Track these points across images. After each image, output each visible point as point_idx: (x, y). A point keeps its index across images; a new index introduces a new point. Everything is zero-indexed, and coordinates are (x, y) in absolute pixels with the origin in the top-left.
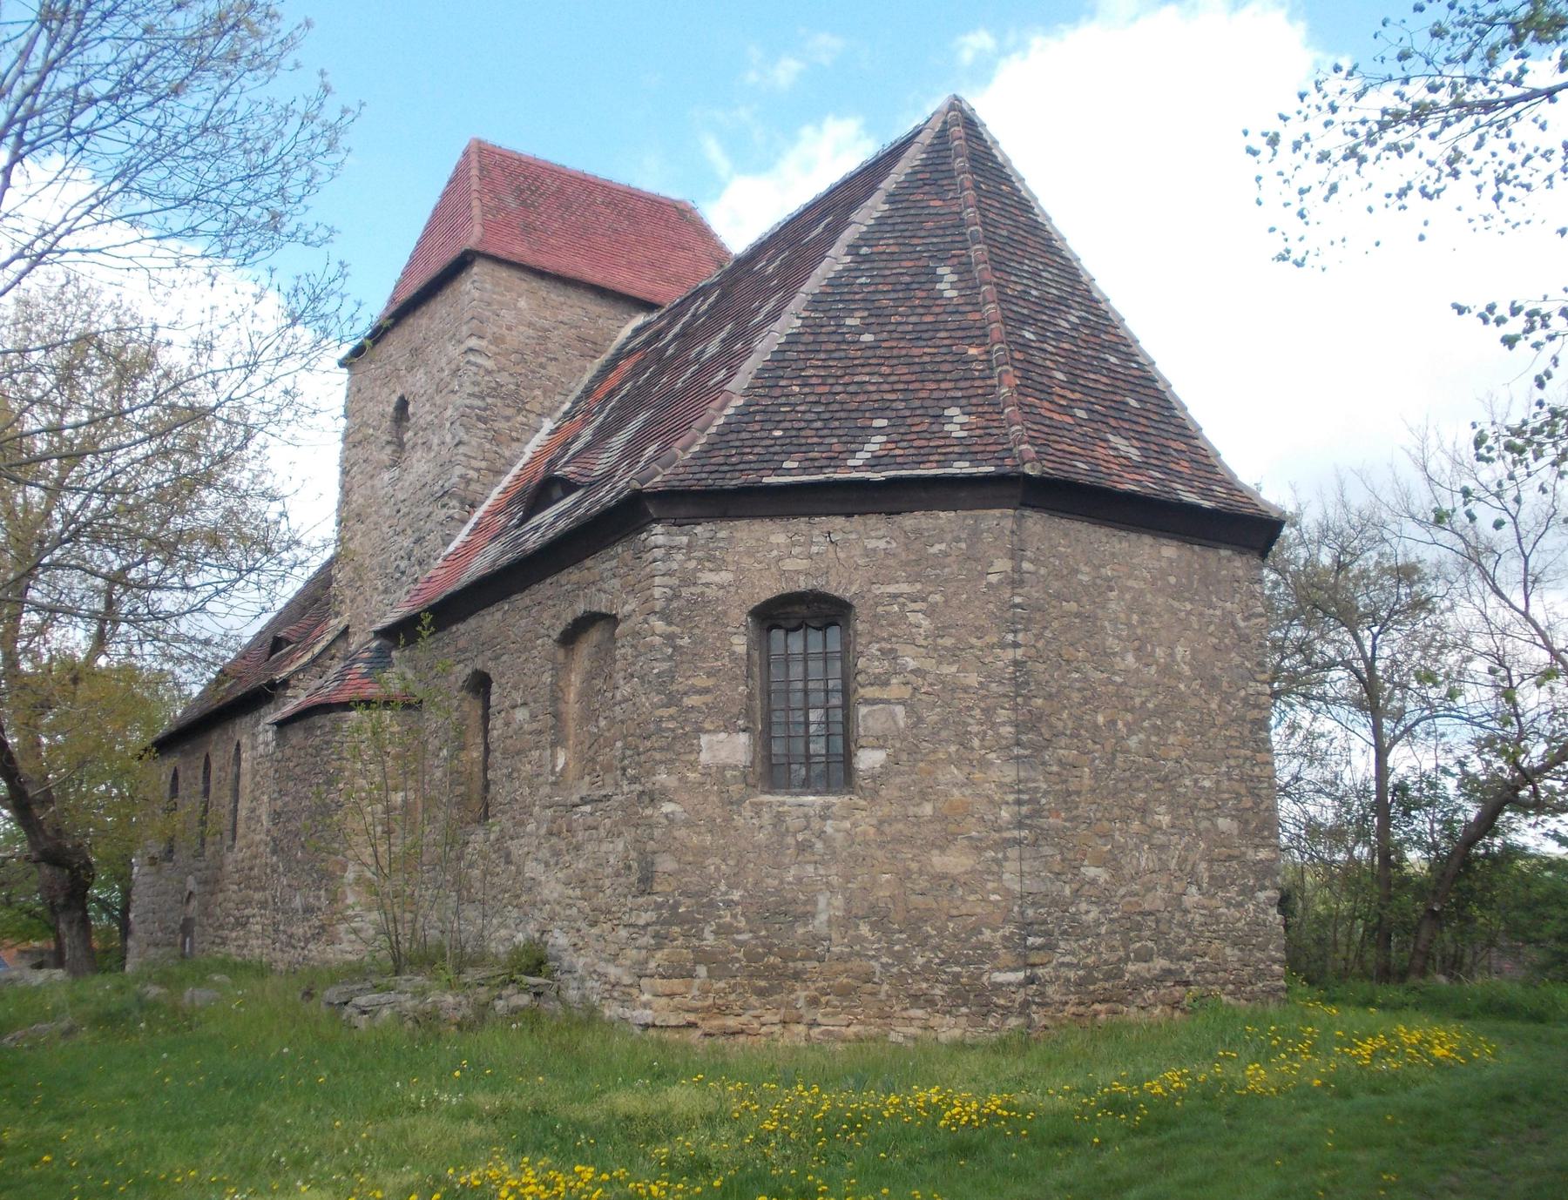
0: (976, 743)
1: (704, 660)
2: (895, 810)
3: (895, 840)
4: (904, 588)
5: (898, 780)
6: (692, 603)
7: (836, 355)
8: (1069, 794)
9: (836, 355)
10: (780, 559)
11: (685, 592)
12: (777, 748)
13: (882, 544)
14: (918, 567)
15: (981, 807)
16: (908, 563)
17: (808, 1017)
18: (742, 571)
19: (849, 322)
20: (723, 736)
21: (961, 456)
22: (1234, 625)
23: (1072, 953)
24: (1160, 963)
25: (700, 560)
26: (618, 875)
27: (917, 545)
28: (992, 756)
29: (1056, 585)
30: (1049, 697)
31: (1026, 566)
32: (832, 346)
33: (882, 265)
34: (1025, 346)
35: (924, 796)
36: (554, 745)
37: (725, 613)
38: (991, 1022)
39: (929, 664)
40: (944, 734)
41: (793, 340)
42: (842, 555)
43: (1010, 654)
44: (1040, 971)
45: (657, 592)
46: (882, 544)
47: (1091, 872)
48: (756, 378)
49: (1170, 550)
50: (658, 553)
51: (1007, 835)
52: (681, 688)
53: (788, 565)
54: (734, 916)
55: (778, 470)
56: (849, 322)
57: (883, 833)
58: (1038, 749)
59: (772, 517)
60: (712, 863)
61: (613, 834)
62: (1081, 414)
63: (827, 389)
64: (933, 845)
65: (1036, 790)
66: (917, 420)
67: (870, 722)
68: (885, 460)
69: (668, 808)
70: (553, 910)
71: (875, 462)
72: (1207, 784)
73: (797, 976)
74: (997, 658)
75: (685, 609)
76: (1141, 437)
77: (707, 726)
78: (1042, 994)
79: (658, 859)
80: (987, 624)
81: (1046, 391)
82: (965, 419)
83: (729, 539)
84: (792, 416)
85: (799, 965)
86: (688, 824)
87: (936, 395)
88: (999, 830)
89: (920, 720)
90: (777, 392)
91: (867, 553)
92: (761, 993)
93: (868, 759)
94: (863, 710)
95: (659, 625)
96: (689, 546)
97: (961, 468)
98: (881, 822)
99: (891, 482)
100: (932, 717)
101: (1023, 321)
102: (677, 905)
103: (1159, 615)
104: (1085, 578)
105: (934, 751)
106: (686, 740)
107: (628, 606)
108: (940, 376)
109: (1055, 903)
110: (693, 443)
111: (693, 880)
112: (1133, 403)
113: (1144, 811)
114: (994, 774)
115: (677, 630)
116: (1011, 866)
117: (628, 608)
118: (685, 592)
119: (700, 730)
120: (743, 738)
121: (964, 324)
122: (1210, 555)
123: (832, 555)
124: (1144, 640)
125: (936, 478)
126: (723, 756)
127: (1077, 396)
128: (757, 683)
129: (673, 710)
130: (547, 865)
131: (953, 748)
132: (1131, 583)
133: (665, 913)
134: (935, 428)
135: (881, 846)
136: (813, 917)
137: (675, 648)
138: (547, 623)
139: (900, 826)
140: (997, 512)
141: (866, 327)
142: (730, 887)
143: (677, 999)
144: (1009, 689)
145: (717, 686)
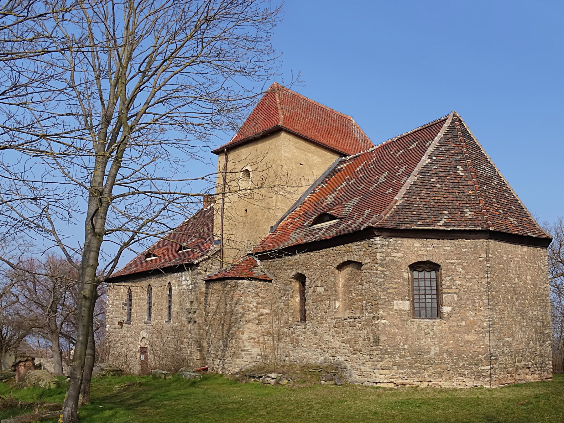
0: (477, 305)
1: (394, 279)
2: (454, 323)
3: (454, 332)
4: (456, 261)
5: (455, 315)
6: (390, 262)
7: (430, 190)
8: (501, 318)
9: (430, 190)
10: (418, 251)
11: (387, 258)
12: (417, 305)
13: (449, 248)
14: (459, 255)
15: (479, 322)
16: (456, 254)
17: (429, 380)
18: (406, 254)
19: (432, 180)
20: (401, 301)
21: (471, 224)
22: (541, 268)
23: (502, 361)
24: (523, 363)
25: (392, 249)
26: (364, 340)
27: (459, 249)
28: (482, 308)
29: (498, 260)
30: (496, 292)
31: (490, 255)
32: (428, 187)
33: (440, 163)
34: (484, 191)
35: (463, 320)
36: (335, 300)
37: (401, 266)
38: (481, 379)
39: (464, 283)
40: (468, 302)
41: (415, 184)
42: (437, 251)
43: (486, 280)
44: (494, 366)
45: (378, 258)
46: (449, 248)
47: (506, 339)
48: (405, 194)
49: (525, 249)
50: (378, 246)
51: (486, 330)
52: (387, 287)
53: (420, 253)
54: (405, 353)
55: (416, 225)
56: (432, 180)
57: (451, 330)
58: (494, 306)
59: (415, 238)
60: (398, 338)
61: (363, 328)
62: (501, 211)
63: (428, 200)
64: (465, 333)
65: (494, 317)
66: (457, 212)
67: (447, 299)
68: (449, 224)
69: (383, 321)
70: (337, 350)
71: (446, 224)
72: (535, 313)
73: (425, 369)
74: (483, 281)
75: (389, 264)
76: (517, 217)
77: (396, 298)
78: (495, 372)
79: (381, 336)
80: (480, 272)
81: (491, 205)
82: (470, 213)
83: (401, 244)
84: (418, 208)
85: (426, 366)
86: (390, 326)
87: (461, 205)
88: (484, 328)
89: (461, 298)
90: (412, 200)
91: (444, 250)
92: (413, 374)
93: (446, 309)
94: (444, 296)
95: (380, 268)
96: (388, 244)
97: (471, 228)
98: (450, 327)
99: (451, 230)
100: (465, 297)
101: (483, 184)
102: (387, 349)
103: (523, 268)
104: (505, 258)
105: (465, 307)
106: (390, 301)
107: (366, 261)
108: (462, 199)
109: (498, 348)
110: (387, 213)
111: (392, 342)
112: (513, 207)
113: (520, 322)
114: (482, 313)
115: (385, 270)
116: (487, 338)
117: (366, 261)
118: (387, 258)
119: (393, 299)
120: (407, 302)
121: (467, 184)
122: (535, 249)
123: (434, 251)
124: (520, 275)
125: (465, 230)
126: (401, 307)
127: (499, 206)
128: (410, 287)
129: (385, 293)
130: (333, 336)
131: (471, 306)
132: (516, 259)
133: (383, 352)
134: (462, 215)
135: (450, 333)
136: (430, 353)
137: (385, 275)
138: (331, 262)
139: (456, 328)
140: (482, 240)
141: (438, 182)
142: (404, 344)
143: (387, 375)
144: (486, 290)
145: (399, 287)
